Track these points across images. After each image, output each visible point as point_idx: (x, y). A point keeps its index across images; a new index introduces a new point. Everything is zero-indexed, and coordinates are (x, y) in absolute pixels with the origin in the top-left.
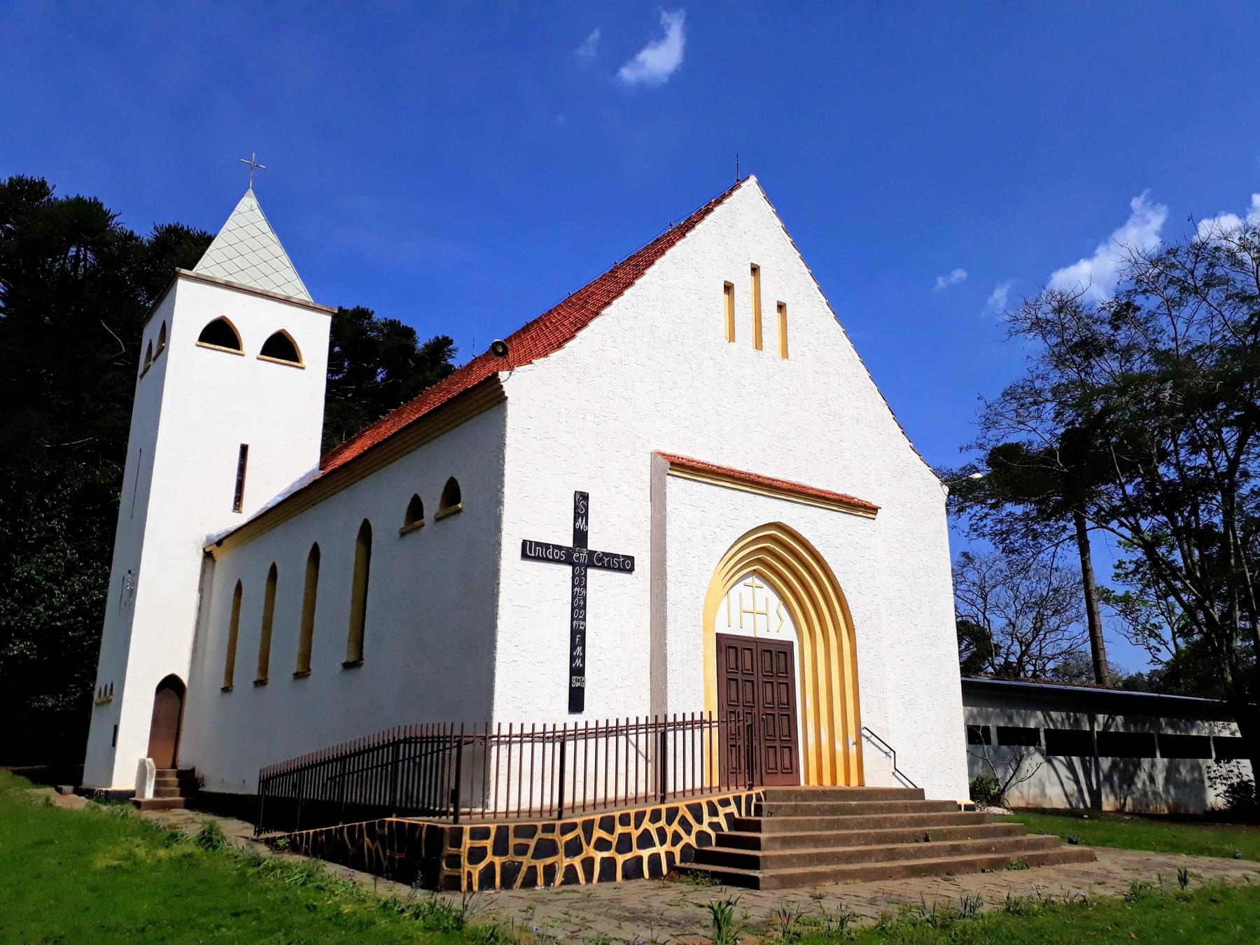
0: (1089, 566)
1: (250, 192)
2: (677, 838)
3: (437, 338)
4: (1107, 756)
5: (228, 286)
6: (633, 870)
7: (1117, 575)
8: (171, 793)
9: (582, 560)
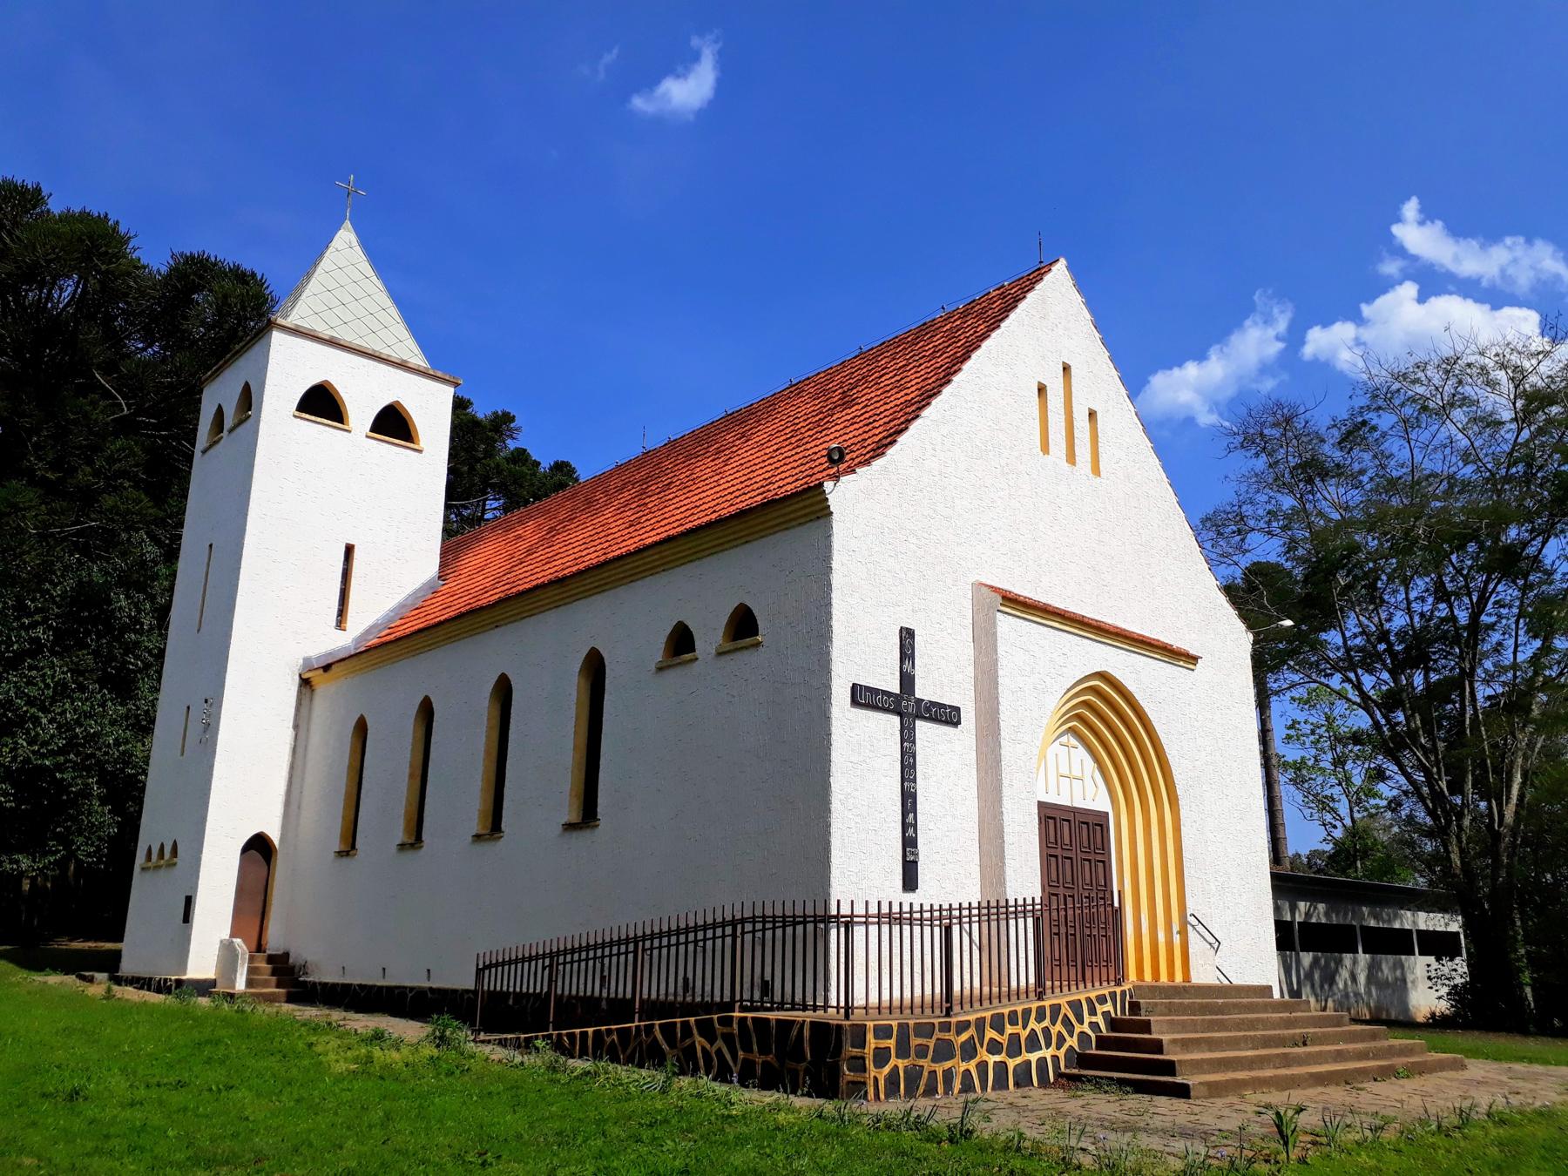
0: (1269, 726)
1: (348, 224)
2: (1061, 1040)
3: (495, 413)
4: (1308, 951)
5: (332, 343)
6: (1023, 1078)
7: (1289, 737)
8: (266, 984)
9: (910, 710)
